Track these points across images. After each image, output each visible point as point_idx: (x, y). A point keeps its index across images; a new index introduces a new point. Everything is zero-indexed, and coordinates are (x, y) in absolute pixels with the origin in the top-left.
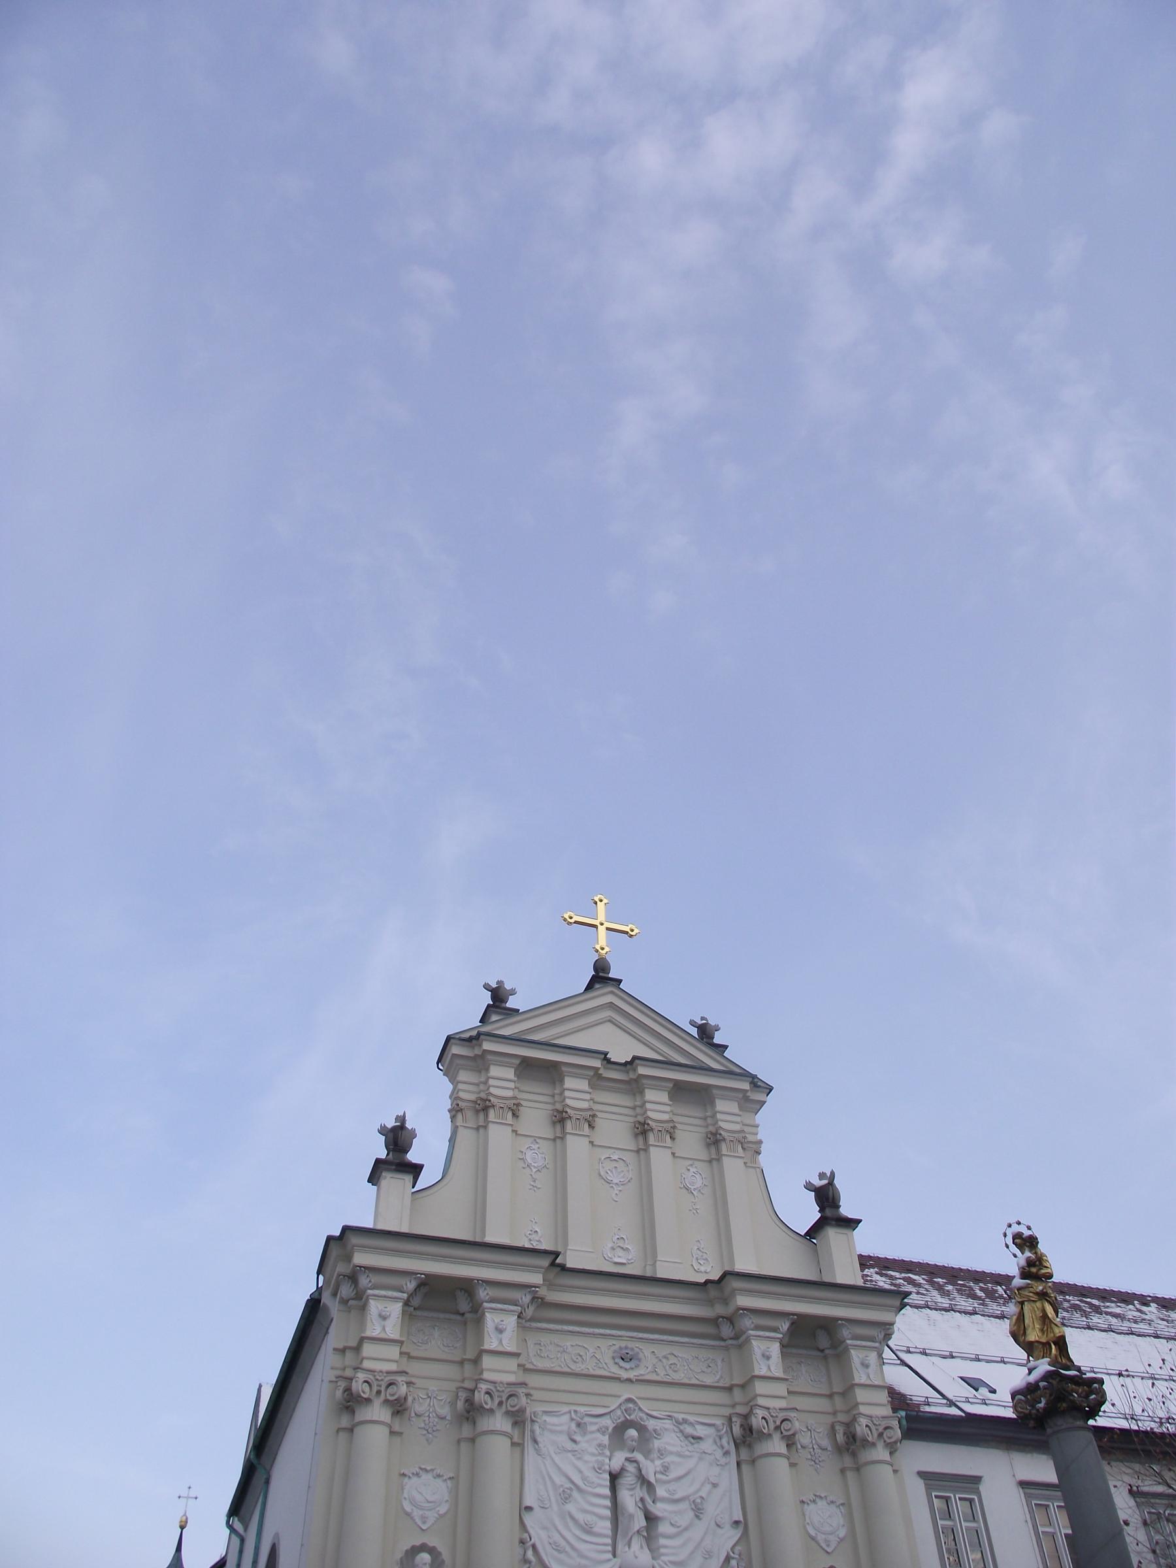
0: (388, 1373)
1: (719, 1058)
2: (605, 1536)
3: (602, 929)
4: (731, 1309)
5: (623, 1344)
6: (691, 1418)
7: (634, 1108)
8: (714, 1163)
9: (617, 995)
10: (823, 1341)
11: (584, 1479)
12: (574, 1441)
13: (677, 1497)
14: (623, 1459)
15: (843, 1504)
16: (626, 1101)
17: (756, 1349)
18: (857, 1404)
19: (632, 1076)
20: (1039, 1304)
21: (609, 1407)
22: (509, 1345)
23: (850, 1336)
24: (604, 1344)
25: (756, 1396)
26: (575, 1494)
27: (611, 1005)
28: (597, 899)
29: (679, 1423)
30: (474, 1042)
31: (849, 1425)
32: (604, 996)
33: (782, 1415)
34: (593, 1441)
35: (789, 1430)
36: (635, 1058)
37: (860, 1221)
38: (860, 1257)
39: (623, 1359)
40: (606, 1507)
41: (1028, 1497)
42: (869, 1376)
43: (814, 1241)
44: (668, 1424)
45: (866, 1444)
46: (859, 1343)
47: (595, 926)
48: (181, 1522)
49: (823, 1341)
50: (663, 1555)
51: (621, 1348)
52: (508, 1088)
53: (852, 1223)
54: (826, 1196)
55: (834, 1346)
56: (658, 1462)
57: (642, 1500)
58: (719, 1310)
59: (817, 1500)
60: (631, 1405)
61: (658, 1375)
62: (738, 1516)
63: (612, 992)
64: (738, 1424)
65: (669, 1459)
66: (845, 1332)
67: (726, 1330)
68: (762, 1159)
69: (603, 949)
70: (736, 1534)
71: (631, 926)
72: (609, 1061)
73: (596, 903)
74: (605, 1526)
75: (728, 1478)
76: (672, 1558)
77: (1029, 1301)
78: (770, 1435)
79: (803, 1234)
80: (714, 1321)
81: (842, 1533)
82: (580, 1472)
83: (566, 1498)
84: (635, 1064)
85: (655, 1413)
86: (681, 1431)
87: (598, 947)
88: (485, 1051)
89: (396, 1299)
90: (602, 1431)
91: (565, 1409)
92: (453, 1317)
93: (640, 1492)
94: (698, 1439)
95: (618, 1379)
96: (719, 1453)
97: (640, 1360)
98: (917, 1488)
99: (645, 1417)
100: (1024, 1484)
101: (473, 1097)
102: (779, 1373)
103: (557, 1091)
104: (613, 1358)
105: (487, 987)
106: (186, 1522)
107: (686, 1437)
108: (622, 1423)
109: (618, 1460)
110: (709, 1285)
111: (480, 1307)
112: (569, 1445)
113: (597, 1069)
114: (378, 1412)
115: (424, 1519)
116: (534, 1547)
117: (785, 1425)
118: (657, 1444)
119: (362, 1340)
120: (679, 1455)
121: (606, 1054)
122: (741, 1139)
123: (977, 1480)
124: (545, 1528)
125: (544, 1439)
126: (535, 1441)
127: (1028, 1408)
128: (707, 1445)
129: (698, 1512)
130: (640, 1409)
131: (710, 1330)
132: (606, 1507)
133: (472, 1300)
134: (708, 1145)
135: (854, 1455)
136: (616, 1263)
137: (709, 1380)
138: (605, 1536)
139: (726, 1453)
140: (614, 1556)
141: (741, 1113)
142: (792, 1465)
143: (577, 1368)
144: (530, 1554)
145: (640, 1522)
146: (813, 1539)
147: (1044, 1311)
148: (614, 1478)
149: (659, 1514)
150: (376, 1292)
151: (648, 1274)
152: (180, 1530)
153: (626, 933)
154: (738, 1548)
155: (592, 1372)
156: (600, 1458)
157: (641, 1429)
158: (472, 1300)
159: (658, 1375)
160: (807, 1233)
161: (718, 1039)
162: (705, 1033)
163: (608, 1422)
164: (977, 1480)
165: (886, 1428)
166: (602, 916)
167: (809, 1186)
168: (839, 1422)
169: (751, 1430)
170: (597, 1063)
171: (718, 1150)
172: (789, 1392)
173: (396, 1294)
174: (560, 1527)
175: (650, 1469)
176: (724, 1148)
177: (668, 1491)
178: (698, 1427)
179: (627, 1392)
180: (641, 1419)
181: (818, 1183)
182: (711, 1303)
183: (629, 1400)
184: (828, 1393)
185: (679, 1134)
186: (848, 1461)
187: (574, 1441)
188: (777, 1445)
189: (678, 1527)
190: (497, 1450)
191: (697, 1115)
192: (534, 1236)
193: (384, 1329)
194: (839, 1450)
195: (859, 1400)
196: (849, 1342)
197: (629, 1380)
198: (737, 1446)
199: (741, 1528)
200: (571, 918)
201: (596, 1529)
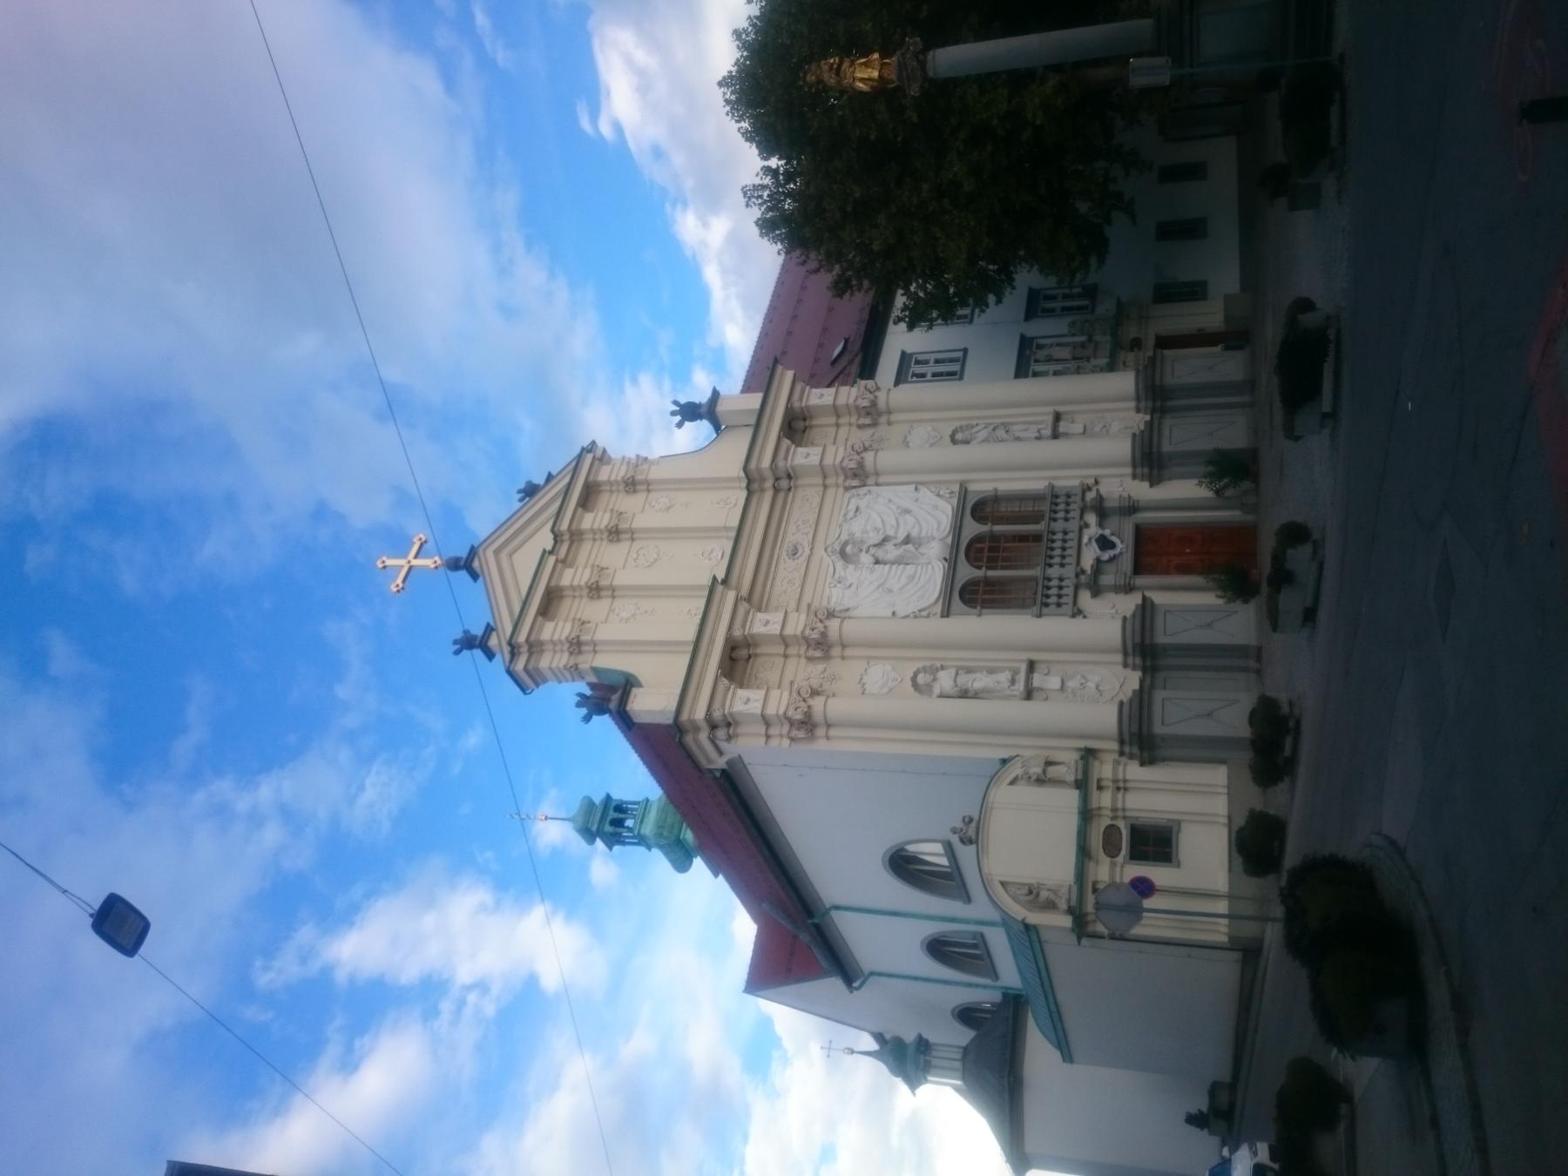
0: (846, 449)
1: (558, 479)
3: (415, 562)
4: (768, 474)
5: (784, 553)
6: (843, 512)
7: (555, 652)
9: (490, 545)
12: (850, 586)
13: (895, 524)
14: (867, 555)
15: (868, 663)
16: (586, 547)
18: (847, 405)
19: (566, 537)
20: (857, 66)
22: (780, 616)
23: (784, 462)
24: (782, 565)
25: (834, 465)
27: (497, 552)
28: (381, 566)
29: (845, 520)
30: (516, 651)
31: (808, 642)
33: (794, 694)
34: (851, 573)
36: (552, 530)
38: (743, 391)
39: (796, 554)
41: (906, 382)
42: (776, 623)
43: (723, 427)
44: (845, 527)
47: (411, 568)
48: (848, 1053)
49: (743, 653)
50: (932, 533)
52: (564, 627)
53: (715, 395)
54: (689, 412)
55: (748, 646)
56: (871, 534)
58: (769, 484)
62: (913, 487)
63: (484, 550)
64: (851, 481)
65: (869, 527)
67: (784, 483)
68: (650, 457)
69: (435, 562)
72: (551, 552)
73: (385, 567)
77: (854, 72)
79: (715, 435)
80: (776, 490)
81: (889, 668)
84: (557, 533)
85: (837, 536)
86: (851, 519)
87: (433, 566)
88: (527, 640)
93: (889, 546)
94: (857, 509)
95: (810, 556)
96: (868, 497)
97: (797, 543)
100: (897, 383)
101: (566, 655)
103: (590, 536)
104: (794, 559)
105: (457, 653)
106: (848, 1049)
107: (855, 516)
108: (841, 555)
109: (866, 559)
111: (747, 640)
113: (557, 561)
114: (817, 703)
115: (895, 680)
116: (920, 611)
117: (856, 447)
118: (858, 535)
119: (763, 716)
122: (580, 623)
125: (847, 603)
126: (847, 610)
127: (899, 139)
128: (862, 504)
129: (907, 511)
131: (781, 496)
134: (635, 491)
136: (722, 556)
137: (817, 500)
139: (869, 492)
140: (929, 563)
141: (575, 567)
142: (834, 695)
144: (924, 613)
146: (890, 690)
147: (861, 64)
148: (877, 562)
149: (905, 534)
150: (727, 707)
151: (734, 534)
153: (422, 544)
154: (933, 489)
155: (803, 574)
157: (846, 543)
161: (539, 480)
162: (530, 491)
163: (840, 564)
164: (904, 356)
165: (799, 694)
168: (806, 652)
169: (803, 723)
170: (552, 559)
171: (625, 532)
172: (779, 688)
173: (751, 616)
175: (874, 538)
179: (819, 551)
181: (584, 711)
182: (762, 490)
184: (822, 489)
185: (604, 565)
187: (850, 586)
188: (817, 703)
190: (851, 629)
191: (589, 547)
192: (693, 612)
193: (756, 700)
194: (827, 657)
195: (775, 712)
197: (811, 549)
198: (864, 485)
199: (919, 486)
200: (398, 586)
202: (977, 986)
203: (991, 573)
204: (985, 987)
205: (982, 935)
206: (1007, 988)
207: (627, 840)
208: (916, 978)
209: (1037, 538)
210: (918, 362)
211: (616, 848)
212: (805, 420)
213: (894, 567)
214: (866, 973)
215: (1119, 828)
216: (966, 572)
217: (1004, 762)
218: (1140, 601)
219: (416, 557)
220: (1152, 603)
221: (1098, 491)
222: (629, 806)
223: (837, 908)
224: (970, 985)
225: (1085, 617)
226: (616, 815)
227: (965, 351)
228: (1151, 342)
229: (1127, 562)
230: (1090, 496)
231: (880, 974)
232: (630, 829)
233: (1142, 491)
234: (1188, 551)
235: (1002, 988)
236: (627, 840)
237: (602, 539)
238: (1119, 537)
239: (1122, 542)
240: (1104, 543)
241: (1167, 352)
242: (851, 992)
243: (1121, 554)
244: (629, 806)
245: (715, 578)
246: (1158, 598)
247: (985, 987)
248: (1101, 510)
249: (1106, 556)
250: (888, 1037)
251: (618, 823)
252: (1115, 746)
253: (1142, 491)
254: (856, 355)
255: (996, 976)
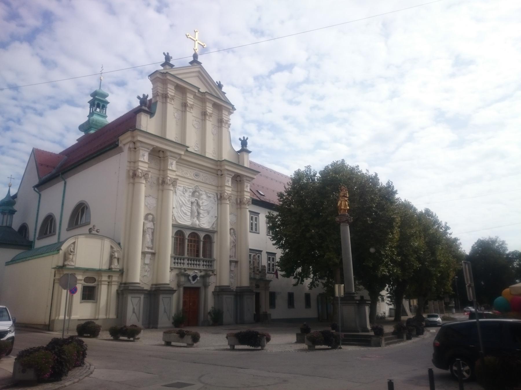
2: (189, 216)
3: (196, 42)
8: (203, 121)
10: (161, 155)
11: (186, 203)
17: (141, 152)
21: (192, 187)
26: (184, 206)
28: (196, 31)
32: (196, 69)
35: (147, 177)
36: (206, 92)
37: (251, 152)
40: (190, 210)
43: (239, 154)
45: (225, 199)
46: (228, 175)
49: (161, 155)
51: (196, 173)
57: (197, 209)
58: (219, 168)
59: (150, 196)
60: (197, 187)
61: (203, 180)
65: (203, 201)
66: (245, 179)
70: (215, 219)
71: (204, 44)
72: (199, 91)
74: (189, 214)
75: (215, 207)
76: (202, 222)
78: (141, 177)
82: (185, 201)
83: (181, 206)
86: (207, 195)
89: (147, 151)
90: (190, 192)
91: (182, 186)
92: (157, 157)
94: (210, 197)
96: (214, 201)
97: (199, 176)
98: (248, 213)
99: (200, 190)
101: (162, 92)
102: (230, 185)
105: (164, 54)
109: (193, 200)
110: (219, 162)
112: (183, 194)
113: (196, 93)
118: (202, 197)
120: (206, 200)
121: (199, 89)
123: (259, 214)
124: (177, 213)
130: (199, 189)
132: (190, 210)
133: (135, 145)
134: (202, 115)
135: (240, 205)
138: (189, 216)
139: (216, 201)
143: (186, 176)
145: (196, 214)
152: (8, 188)
156: (189, 198)
158: (135, 145)
159: (203, 180)
160: (237, 152)
163: (191, 190)
164: (259, 214)
166: (197, 38)
167: (139, 98)
174: (181, 214)
176: (168, 100)
177: (203, 208)
178: (211, 195)
180: (199, 191)
181: (142, 97)
182: (217, 166)
183: (197, 186)
186: (131, 180)
189: (204, 216)
195: (245, 194)
196: (245, 181)
197: (197, 181)
201: (188, 214)
202: (35, 232)
203: (186, 241)
204: (35, 235)
205: (55, 234)
206: (34, 243)
207: (92, 108)
208: (38, 211)
209: (198, 255)
210: (256, 218)
211: (89, 104)
212: (240, 181)
213: (190, 209)
214: (40, 193)
215: (95, 282)
216: (187, 233)
217: (119, 244)
218: (174, 289)
219: (198, 43)
220: (174, 293)
221: (212, 275)
222: (104, 110)
223: (65, 183)
224: (36, 230)
225: (170, 271)
226: (101, 105)
227: (259, 233)
228: (258, 291)
229: (188, 285)
230: (211, 273)
231: (40, 198)
232: (96, 110)
233: (211, 289)
234: (191, 304)
235: (34, 241)
236: (92, 108)
237: (203, 109)
238: (196, 282)
239: (195, 283)
240: (195, 277)
241: (254, 296)
242: (33, 187)
243: (191, 283)
244: (104, 110)
245: (188, 147)
246: (175, 296)
247: (35, 235)
248: (205, 277)
249: (190, 278)
250: (15, 200)
251: (98, 106)
252: (124, 281)
253: (211, 289)
254: (259, 198)
255: (38, 239)
